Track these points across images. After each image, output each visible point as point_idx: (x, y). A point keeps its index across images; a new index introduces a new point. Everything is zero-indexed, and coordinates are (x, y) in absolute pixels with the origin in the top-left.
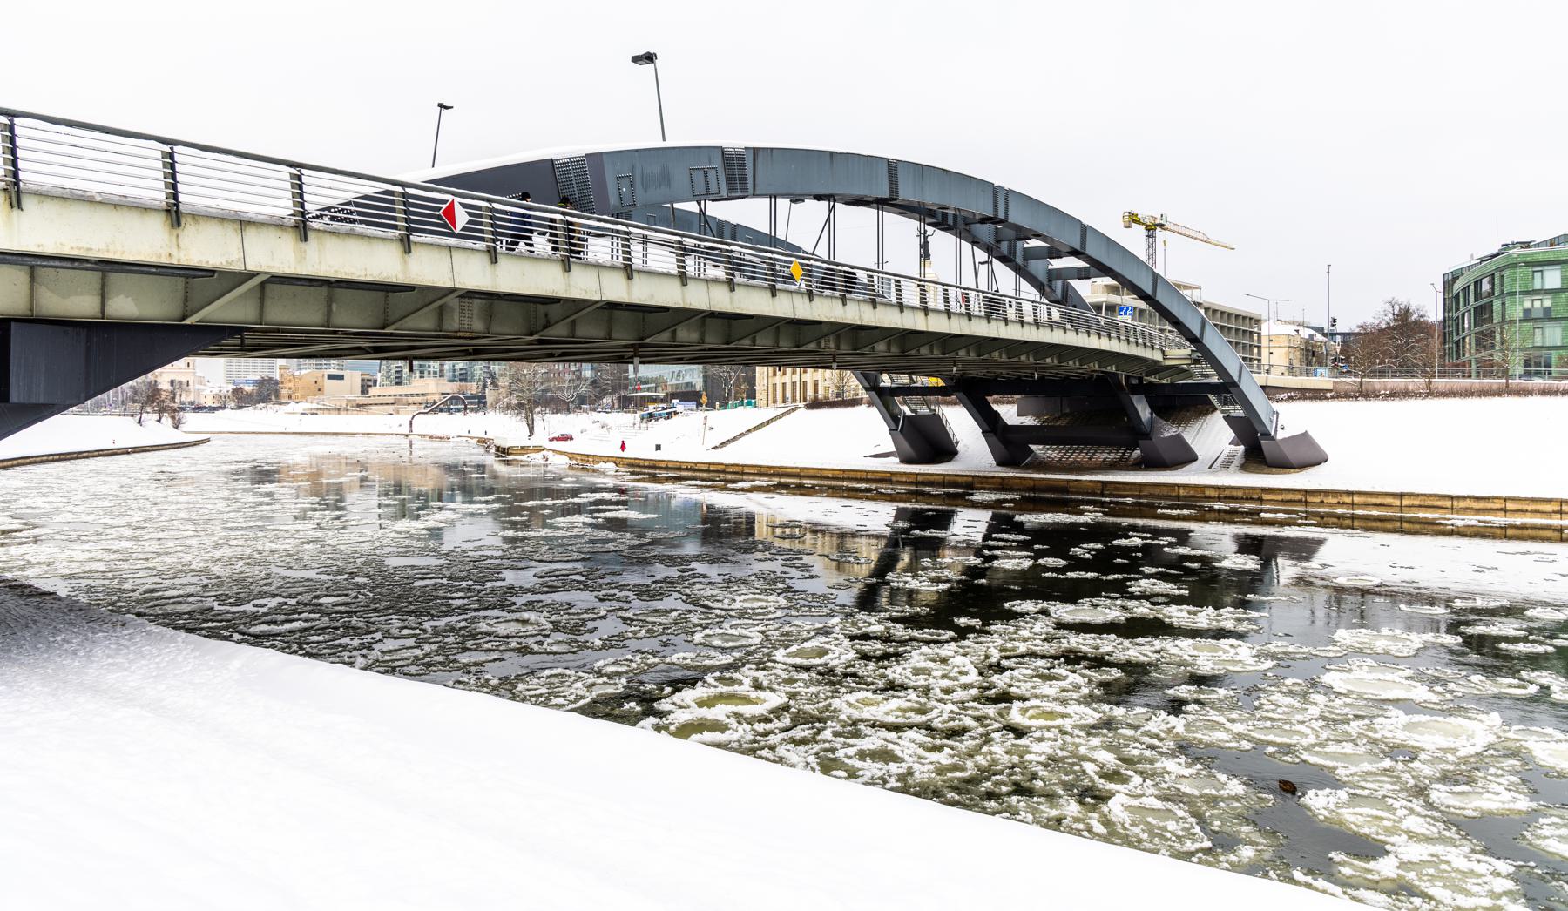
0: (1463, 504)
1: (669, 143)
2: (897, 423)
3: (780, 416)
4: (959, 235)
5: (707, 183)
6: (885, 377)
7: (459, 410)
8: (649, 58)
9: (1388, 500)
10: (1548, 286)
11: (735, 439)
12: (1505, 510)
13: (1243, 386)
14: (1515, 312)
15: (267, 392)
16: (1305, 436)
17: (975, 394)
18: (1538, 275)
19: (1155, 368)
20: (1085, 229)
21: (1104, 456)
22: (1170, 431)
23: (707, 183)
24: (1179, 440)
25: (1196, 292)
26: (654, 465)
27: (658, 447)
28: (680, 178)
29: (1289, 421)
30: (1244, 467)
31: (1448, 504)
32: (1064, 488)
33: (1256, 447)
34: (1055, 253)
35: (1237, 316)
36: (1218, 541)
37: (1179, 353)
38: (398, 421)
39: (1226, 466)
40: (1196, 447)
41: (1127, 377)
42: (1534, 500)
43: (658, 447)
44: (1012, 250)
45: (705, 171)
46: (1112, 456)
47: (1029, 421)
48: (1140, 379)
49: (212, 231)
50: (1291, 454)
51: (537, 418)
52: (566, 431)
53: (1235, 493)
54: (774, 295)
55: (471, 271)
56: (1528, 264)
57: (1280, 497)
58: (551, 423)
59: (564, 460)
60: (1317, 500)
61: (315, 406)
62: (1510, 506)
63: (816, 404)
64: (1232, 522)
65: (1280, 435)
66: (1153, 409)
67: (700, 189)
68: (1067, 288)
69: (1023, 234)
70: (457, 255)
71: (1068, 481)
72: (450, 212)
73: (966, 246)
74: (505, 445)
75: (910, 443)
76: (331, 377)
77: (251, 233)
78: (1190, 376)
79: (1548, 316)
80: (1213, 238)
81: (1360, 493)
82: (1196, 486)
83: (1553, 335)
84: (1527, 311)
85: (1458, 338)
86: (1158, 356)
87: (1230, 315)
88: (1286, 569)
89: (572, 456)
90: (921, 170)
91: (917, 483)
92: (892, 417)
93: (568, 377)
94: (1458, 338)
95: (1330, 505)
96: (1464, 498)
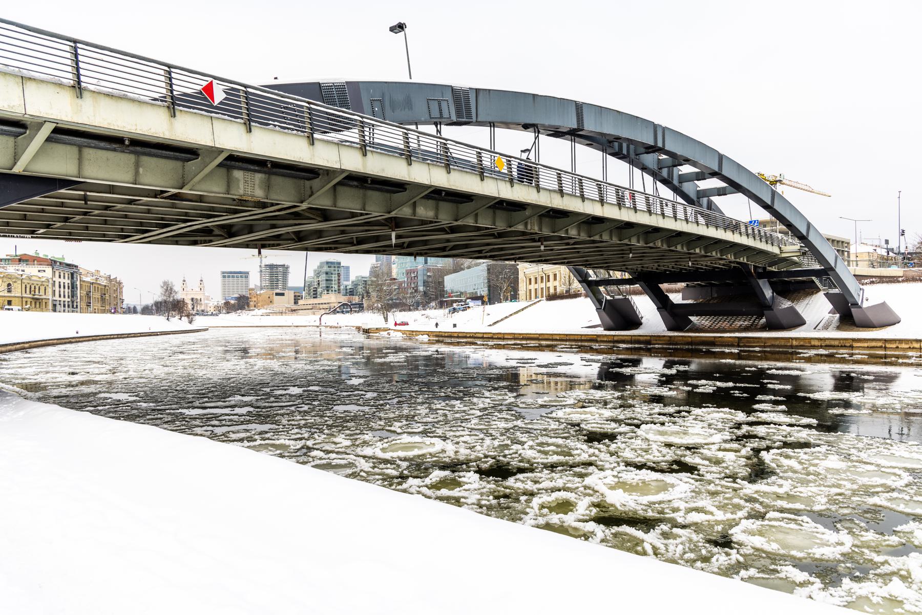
2: (601, 305)
4: (632, 163)
5: (441, 110)
6: (591, 272)
7: (348, 312)
8: (401, 27)
13: (837, 270)
16: (883, 305)
17: (651, 283)
20: (721, 157)
22: (786, 304)
23: (441, 110)
24: (792, 310)
29: (871, 297)
30: (839, 328)
33: (847, 313)
34: (700, 176)
36: (820, 378)
38: (310, 319)
39: (826, 328)
40: (804, 315)
41: (755, 267)
43: (455, 326)
44: (671, 174)
46: (746, 323)
48: (764, 268)
50: (873, 318)
51: (390, 314)
52: (405, 320)
53: (833, 343)
54: (482, 180)
57: (866, 345)
58: (399, 316)
59: (400, 334)
61: (268, 311)
63: (552, 297)
64: (830, 362)
66: (774, 291)
67: (435, 113)
68: (710, 205)
69: (678, 160)
71: (715, 337)
73: (637, 172)
76: (277, 294)
82: (805, 339)
86: (776, 250)
90: (601, 111)
92: (598, 300)
93: (410, 291)
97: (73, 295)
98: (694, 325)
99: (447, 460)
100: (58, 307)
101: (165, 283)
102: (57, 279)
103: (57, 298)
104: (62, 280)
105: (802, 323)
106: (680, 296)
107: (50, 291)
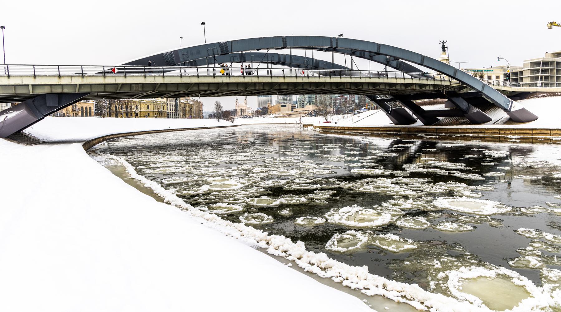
0: (554, 132)
9: (528, 132)
15: (264, 112)
27: (336, 123)
31: (549, 132)
49: (66, 78)
55: (140, 80)
57: (491, 132)
60: (503, 132)
70: (116, 78)
75: (395, 118)
76: (282, 106)
96: (555, 130)
97: (176, 109)
99: (334, 222)
100: (169, 116)
101: (217, 102)
102: (169, 102)
103: (169, 111)
104: (171, 103)
105: (490, 120)
106: (444, 105)
107: (165, 108)
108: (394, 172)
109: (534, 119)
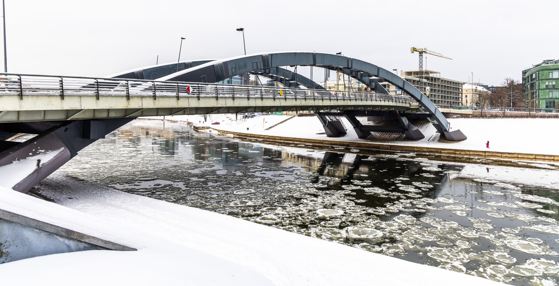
0: (505, 155)
1: (247, 56)
3: (289, 119)
9: (481, 153)
10: (554, 77)
11: (274, 126)
12: (518, 158)
13: (436, 115)
14: (543, 86)
18: (551, 73)
19: (408, 109)
21: (394, 136)
22: (415, 128)
24: (418, 131)
25: (438, 74)
26: (246, 135)
27: (248, 129)
28: (249, 67)
29: (454, 125)
30: (440, 141)
31: (500, 155)
32: (378, 147)
35: (454, 83)
37: (415, 104)
39: (433, 140)
41: (399, 112)
42: (527, 154)
43: (248, 129)
45: (257, 63)
47: (371, 123)
48: (404, 112)
50: (454, 137)
53: (432, 150)
56: (547, 69)
59: (217, 132)
62: (520, 156)
65: (450, 131)
70: (190, 99)
72: (188, 89)
74: (197, 126)
77: (144, 99)
78: (420, 111)
79: (554, 88)
80: (444, 56)
81: (472, 151)
83: (555, 94)
84: (547, 86)
85: (513, 98)
86: (408, 105)
87: (451, 82)
88: (453, 175)
89: (219, 131)
91: (331, 144)
92: (324, 121)
94: (513, 98)
95: (463, 155)
96: (505, 153)
98: (372, 135)
105: (422, 137)
108: (362, 188)
109: (463, 138)
